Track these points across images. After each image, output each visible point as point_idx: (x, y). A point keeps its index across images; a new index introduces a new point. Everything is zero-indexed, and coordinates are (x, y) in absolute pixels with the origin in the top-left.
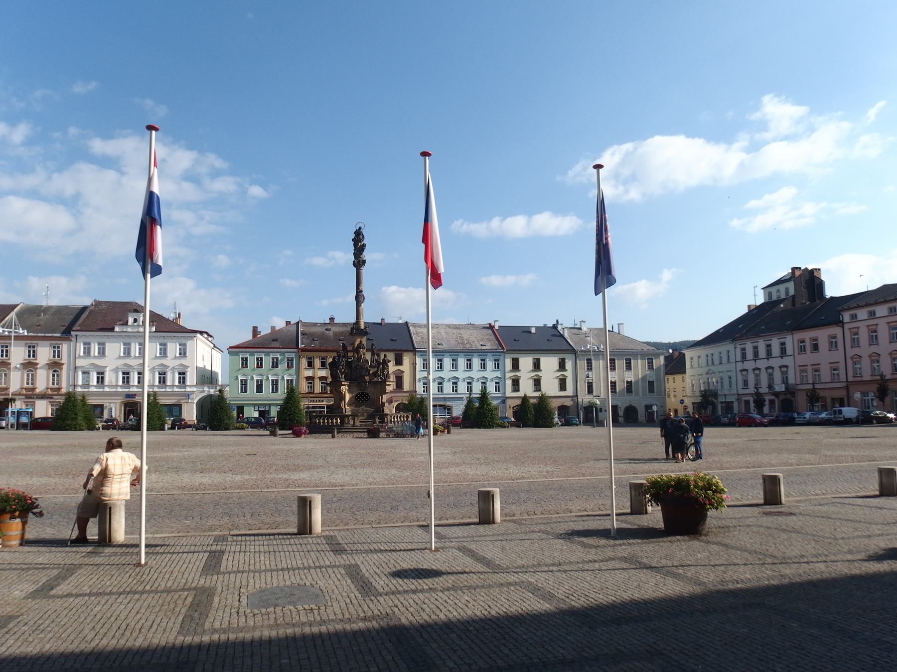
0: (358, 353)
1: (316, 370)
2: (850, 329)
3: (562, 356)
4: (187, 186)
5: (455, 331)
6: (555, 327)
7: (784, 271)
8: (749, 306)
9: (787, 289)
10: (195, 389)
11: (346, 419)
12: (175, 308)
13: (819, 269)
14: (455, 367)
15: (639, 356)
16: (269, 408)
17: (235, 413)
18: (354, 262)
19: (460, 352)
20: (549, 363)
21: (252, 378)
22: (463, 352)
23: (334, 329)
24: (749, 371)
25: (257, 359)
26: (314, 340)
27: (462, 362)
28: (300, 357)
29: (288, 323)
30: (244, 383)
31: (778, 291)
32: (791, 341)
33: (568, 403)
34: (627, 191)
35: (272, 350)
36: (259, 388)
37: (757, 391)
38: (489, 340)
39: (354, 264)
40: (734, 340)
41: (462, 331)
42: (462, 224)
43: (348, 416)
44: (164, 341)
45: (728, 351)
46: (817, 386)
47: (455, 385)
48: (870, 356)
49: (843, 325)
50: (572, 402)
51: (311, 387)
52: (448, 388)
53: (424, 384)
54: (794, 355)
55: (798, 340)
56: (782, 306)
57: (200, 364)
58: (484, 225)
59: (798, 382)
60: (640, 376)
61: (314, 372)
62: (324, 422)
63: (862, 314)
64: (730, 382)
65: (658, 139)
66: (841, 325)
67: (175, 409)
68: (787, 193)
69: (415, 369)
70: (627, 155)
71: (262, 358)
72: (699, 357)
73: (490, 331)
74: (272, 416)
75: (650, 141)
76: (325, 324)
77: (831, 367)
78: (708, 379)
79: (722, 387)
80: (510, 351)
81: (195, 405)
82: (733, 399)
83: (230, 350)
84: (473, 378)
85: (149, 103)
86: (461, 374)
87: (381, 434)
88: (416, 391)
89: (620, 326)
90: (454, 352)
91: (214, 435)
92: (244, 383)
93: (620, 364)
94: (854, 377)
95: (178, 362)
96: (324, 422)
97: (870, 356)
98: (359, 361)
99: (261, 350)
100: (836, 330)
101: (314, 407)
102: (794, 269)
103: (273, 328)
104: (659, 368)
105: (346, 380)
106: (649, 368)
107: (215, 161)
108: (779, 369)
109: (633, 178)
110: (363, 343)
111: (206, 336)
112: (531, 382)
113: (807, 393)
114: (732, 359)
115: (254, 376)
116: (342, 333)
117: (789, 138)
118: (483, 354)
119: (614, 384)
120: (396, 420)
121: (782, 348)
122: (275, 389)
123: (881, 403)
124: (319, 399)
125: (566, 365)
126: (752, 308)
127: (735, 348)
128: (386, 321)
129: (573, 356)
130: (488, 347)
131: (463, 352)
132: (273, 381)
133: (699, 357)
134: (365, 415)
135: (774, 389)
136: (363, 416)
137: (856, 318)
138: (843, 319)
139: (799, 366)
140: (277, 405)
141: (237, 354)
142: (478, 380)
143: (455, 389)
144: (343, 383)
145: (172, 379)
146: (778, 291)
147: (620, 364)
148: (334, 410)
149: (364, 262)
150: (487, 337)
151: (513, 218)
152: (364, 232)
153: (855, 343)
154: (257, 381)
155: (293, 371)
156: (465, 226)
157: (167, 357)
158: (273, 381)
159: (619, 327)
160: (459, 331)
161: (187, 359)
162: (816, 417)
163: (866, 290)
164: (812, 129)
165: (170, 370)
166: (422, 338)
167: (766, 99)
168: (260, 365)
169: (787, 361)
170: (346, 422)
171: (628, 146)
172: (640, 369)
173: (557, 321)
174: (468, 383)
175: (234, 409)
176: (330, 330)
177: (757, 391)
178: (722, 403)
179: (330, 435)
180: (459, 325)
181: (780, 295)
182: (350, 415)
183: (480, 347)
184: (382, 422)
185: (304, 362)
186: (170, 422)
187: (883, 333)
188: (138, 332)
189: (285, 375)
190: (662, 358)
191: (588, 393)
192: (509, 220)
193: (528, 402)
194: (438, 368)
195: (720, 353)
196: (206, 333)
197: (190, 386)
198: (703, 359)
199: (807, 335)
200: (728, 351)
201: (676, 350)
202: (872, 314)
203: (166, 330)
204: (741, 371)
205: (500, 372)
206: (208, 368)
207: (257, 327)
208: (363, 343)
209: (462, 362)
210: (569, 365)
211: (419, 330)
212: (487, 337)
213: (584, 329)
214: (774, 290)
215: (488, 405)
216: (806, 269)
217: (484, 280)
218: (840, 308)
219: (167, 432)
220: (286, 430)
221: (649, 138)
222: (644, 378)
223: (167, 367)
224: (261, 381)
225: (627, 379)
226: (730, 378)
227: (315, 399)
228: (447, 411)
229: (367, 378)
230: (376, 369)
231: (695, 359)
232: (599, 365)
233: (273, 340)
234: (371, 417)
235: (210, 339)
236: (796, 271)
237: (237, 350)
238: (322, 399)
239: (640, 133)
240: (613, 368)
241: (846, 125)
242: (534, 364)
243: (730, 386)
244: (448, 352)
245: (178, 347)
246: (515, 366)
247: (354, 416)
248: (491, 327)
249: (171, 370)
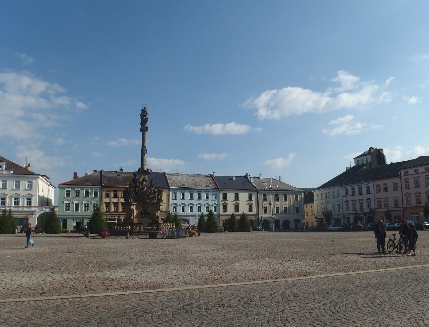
0: (142, 184)
1: (111, 198)
2: (404, 179)
3: (250, 193)
4: (42, 100)
5: (191, 178)
6: (246, 177)
7: (365, 149)
8: (347, 168)
9: (367, 159)
10: (37, 209)
11: (135, 227)
12: (26, 161)
13: (383, 149)
14: (192, 198)
15: (291, 193)
16: (83, 221)
17: (61, 223)
18: (141, 129)
19: (195, 189)
20: (243, 196)
21: (73, 203)
22: (196, 189)
23: (122, 175)
24: (349, 202)
25: (76, 191)
26: (110, 181)
27: (195, 195)
28: (102, 191)
29: (95, 171)
30: (68, 206)
31: (362, 160)
32: (372, 185)
33: (254, 218)
34: (273, 114)
35: (85, 186)
36: (77, 209)
37: (357, 212)
38: (210, 183)
39: (141, 130)
40: (341, 185)
41: (196, 178)
42: (190, 127)
43: (136, 224)
44: (18, 180)
45: (338, 191)
46: (389, 209)
47: (191, 208)
48: (415, 194)
49: (401, 177)
50: (255, 218)
51: (108, 208)
52: (187, 209)
53: (174, 207)
54: (374, 193)
55: (376, 185)
56: (365, 167)
57: (41, 194)
58: (201, 128)
59: (377, 207)
60: (291, 204)
61: (110, 200)
62: (120, 228)
63: (411, 171)
64: (339, 207)
65: (289, 88)
66: (400, 177)
67: (24, 221)
68: (349, 118)
69: (169, 198)
70: (274, 95)
71: (79, 191)
72: (322, 194)
73: (211, 179)
74: (84, 224)
75: (285, 89)
76: (117, 172)
77: (378, 201)
78: (326, 206)
79: (334, 210)
80: (222, 189)
81: (37, 218)
82: (341, 216)
83: (59, 186)
84: (201, 204)
85: (23, 55)
86: (195, 202)
87: (159, 236)
88: (169, 211)
89: (280, 177)
90: (192, 189)
91: (46, 237)
92: (68, 206)
93: (281, 197)
94: (407, 204)
95: (27, 192)
96: (120, 228)
97: (415, 194)
98: (143, 190)
99: (79, 186)
100: (397, 180)
101: (110, 220)
102: (370, 149)
103: (86, 174)
104: (301, 200)
105: (135, 202)
106: (296, 200)
107: (58, 87)
108: (366, 200)
109: (276, 107)
110: (146, 178)
111: (45, 178)
112: (234, 207)
113: (384, 213)
114: (340, 195)
115: (74, 201)
116: (127, 178)
117: (350, 92)
118: (207, 191)
119: (277, 208)
120: (166, 227)
121: (360, 190)
122: (87, 209)
123: (426, 218)
124: (113, 215)
125: (253, 197)
126: (348, 169)
127: (342, 189)
128: (152, 172)
129: (256, 193)
130: (210, 187)
131: (196, 189)
132: (85, 204)
133: (322, 194)
134: (147, 224)
135: (364, 211)
136: (145, 225)
137: (408, 173)
138: (400, 174)
139: (377, 199)
140: (87, 219)
141: (64, 188)
142: (204, 205)
143: (191, 210)
144: (133, 204)
145: (23, 202)
146: (362, 160)
147: (281, 197)
148: (128, 221)
149: (147, 129)
150: (209, 181)
151: (216, 125)
152: (148, 111)
153: (408, 186)
154: (76, 204)
155: (98, 199)
156: (191, 128)
157: (20, 189)
158: (85, 204)
159: (279, 178)
160: (194, 178)
161: (33, 190)
162: (392, 225)
163: (410, 159)
164: (361, 88)
165: (22, 197)
166: (173, 181)
167: (340, 72)
168: (78, 195)
169: (370, 196)
170: (135, 228)
171: (274, 91)
172: (291, 201)
173: (247, 174)
174: (199, 207)
175: (61, 221)
176: (120, 175)
177: (357, 212)
178: (334, 218)
179: (125, 237)
180: (194, 175)
181: (363, 162)
182: (137, 224)
183: (206, 187)
184: (158, 228)
185: (104, 194)
186: (20, 229)
187: (422, 182)
188: (2, 174)
189: (93, 202)
190: (303, 194)
191: (264, 213)
192: (214, 126)
193: (235, 217)
194: (182, 198)
195: (334, 192)
196: (45, 176)
197: (34, 207)
198: (324, 194)
199: (381, 182)
200: (338, 191)
201: (307, 191)
202: (416, 171)
203: (20, 173)
204: (345, 201)
205: (216, 201)
206: (46, 196)
207: (76, 173)
208: (146, 178)
209: (195, 195)
210: (254, 197)
211: (171, 177)
212: (209, 181)
213: (262, 178)
214: (360, 159)
215: (213, 219)
216: (376, 149)
217: (200, 156)
218: (399, 168)
219: (17, 234)
220: (93, 233)
221: (286, 87)
222: (293, 205)
223: (20, 195)
224: (78, 204)
225: (264, 205)
226: (339, 205)
227: (111, 215)
228: (187, 223)
229: (148, 201)
230: (153, 195)
231: (319, 195)
232: (271, 197)
233: (86, 181)
234: (150, 225)
235: (48, 180)
236: (371, 149)
237: (64, 186)
238: (115, 215)
239: (280, 86)
240: (277, 200)
241: (376, 87)
242: (235, 197)
243: (339, 210)
244: (188, 189)
245: (27, 183)
246: (225, 198)
247: (139, 224)
248: (211, 176)
249: (22, 197)
